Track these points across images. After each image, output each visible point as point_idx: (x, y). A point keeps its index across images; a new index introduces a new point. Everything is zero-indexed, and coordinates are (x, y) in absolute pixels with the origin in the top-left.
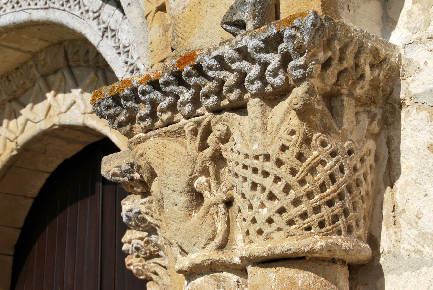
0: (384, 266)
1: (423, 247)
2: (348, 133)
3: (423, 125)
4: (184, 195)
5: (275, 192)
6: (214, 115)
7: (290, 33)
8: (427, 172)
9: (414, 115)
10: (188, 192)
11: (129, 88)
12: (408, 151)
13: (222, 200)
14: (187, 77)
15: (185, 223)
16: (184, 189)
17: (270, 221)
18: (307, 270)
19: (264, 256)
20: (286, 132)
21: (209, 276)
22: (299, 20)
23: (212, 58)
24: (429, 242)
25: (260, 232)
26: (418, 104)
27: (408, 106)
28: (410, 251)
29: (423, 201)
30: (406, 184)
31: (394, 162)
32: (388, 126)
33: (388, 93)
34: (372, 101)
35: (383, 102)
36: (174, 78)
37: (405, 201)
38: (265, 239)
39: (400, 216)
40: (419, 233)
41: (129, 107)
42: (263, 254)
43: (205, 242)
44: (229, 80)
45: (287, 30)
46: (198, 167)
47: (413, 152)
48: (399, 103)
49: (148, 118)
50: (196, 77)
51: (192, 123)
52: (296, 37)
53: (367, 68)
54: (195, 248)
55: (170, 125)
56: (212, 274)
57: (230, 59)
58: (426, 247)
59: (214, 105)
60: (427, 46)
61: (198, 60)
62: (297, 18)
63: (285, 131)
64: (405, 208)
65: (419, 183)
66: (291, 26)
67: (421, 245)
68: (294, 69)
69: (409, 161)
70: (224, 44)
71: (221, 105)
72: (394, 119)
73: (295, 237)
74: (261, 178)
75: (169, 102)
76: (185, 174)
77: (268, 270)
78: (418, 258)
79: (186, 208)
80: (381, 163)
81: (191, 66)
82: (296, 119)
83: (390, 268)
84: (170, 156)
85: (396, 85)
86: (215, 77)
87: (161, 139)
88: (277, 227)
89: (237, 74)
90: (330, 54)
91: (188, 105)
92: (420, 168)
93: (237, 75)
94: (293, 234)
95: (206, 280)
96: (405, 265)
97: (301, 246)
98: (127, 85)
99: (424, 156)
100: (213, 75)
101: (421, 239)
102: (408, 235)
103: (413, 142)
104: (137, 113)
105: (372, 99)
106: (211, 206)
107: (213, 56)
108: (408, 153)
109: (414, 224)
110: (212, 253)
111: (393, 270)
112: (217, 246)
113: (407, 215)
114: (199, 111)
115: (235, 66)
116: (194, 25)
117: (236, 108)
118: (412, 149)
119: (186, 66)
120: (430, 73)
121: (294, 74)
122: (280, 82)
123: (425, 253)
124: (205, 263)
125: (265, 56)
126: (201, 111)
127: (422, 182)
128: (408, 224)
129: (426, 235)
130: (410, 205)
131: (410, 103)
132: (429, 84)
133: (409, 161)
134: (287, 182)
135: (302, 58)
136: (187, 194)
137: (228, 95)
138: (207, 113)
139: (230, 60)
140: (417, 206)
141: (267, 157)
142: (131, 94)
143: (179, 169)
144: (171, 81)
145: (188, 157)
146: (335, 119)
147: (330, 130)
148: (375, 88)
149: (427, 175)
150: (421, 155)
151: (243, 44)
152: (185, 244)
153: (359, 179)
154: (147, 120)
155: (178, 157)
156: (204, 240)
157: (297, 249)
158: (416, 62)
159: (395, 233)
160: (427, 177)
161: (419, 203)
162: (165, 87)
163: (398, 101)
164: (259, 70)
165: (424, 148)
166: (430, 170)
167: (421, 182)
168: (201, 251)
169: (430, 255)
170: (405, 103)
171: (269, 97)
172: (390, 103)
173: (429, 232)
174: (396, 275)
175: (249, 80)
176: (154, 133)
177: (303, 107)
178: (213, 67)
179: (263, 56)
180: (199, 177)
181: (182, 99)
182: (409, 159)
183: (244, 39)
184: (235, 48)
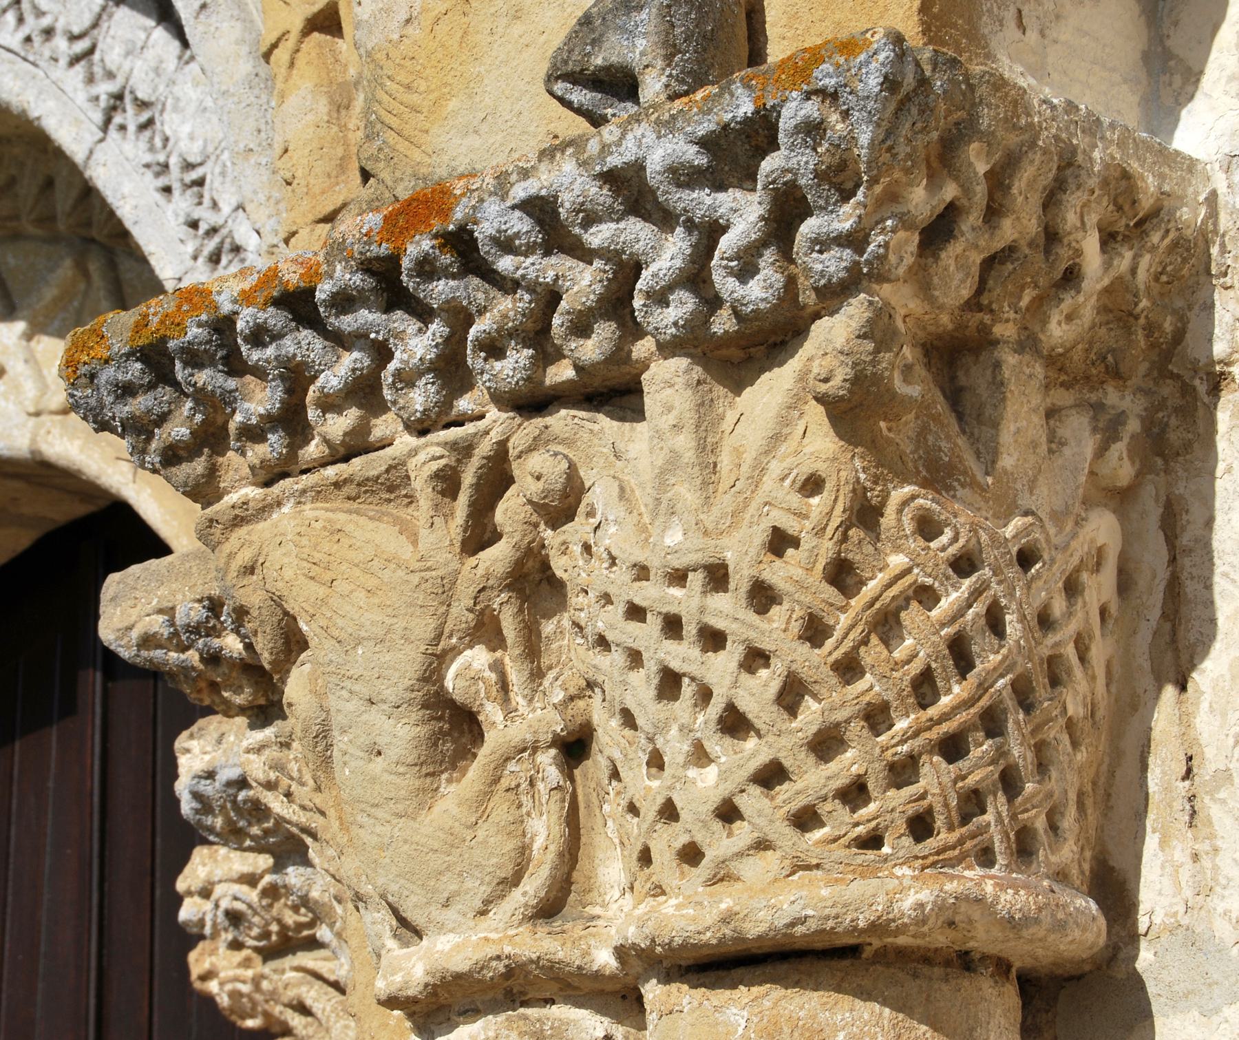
2: (1019, 486)
5: (747, 705)
6: (518, 420)
7: (802, 113)
10: (425, 706)
11: (204, 317)
13: (550, 736)
14: (418, 276)
16: (409, 695)
17: (728, 813)
18: (865, 994)
20: (788, 482)
21: (502, 1017)
22: (838, 66)
23: (513, 207)
31: (1190, 596)
32: (1166, 462)
33: (1169, 337)
34: (1107, 367)
35: (1150, 370)
36: (370, 282)
38: (710, 880)
39: (1211, 793)
41: (203, 389)
42: (702, 937)
43: (484, 891)
44: (576, 289)
45: (794, 104)
46: (461, 613)
48: (1208, 374)
49: (273, 430)
51: (438, 451)
52: (825, 130)
53: (1091, 245)
55: (356, 456)
56: (514, 1010)
57: (579, 211)
59: (521, 383)
61: (459, 214)
63: (783, 479)
64: (1231, 766)
66: (805, 87)
68: (817, 248)
70: (558, 155)
71: (548, 382)
72: (1190, 436)
73: (820, 873)
74: (695, 652)
75: (354, 370)
76: (413, 638)
79: (416, 765)
80: (1140, 597)
81: (436, 236)
82: (826, 435)
83: (1176, 988)
85: (1196, 307)
86: (523, 276)
87: (322, 509)
88: (756, 835)
89: (607, 268)
90: (950, 191)
91: (424, 380)
93: (605, 272)
94: (814, 862)
97: (845, 906)
98: (195, 308)
100: (518, 268)
104: (234, 411)
105: (1110, 358)
106: (508, 759)
107: (516, 201)
111: (1186, 996)
112: (533, 907)
114: (464, 404)
116: (446, 84)
117: (602, 394)
119: (417, 237)
121: (819, 267)
122: (764, 295)
124: (485, 972)
126: (472, 406)
135: (847, 208)
136: (420, 713)
137: (573, 345)
138: (493, 413)
139: (581, 215)
141: (717, 577)
143: (389, 621)
144: (361, 291)
145: (423, 574)
146: (972, 434)
147: (950, 475)
148: (1120, 319)
151: (629, 157)
152: (414, 899)
153: (1061, 656)
154: (269, 436)
155: (386, 575)
157: (827, 918)
159: (1196, 857)
162: (337, 316)
163: (1207, 365)
164: (688, 251)
168: (472, 924)
170: (1230, 373)
171: (724, 352)
172: (1173, 376)
174: (1196, 1013)
175: (652, 287)
178: (517, 242)
179: (702, 201)
181: (402, 361)
183: (630, 136)
184: (598, 168)
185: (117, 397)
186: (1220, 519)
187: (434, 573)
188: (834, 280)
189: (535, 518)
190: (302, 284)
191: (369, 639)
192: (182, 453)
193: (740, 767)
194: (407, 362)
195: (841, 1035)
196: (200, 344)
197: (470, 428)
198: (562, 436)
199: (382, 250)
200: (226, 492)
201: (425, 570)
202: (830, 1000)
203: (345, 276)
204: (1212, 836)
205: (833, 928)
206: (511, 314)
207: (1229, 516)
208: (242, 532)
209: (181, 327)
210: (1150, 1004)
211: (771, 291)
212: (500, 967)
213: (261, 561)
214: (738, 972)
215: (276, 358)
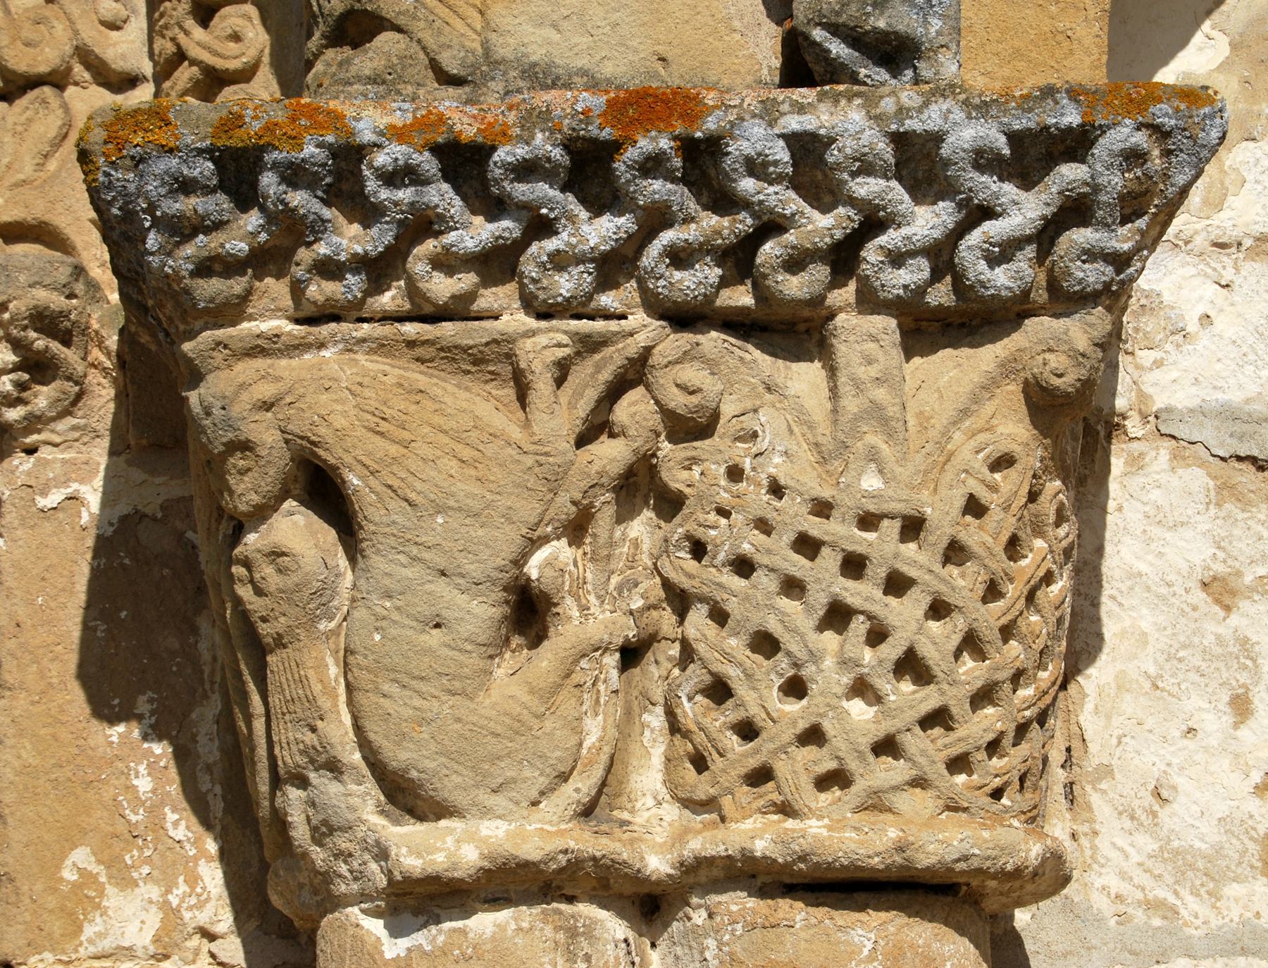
0: (1031, 941)
1: (1176, 893)
3: (1190, 512)
4: (487, 596)
5: (927, 651)
6: (668, 330)
7: (1133, 140)
8: (1197, 661)
9: (1158, 473)
10: (505, 589)
11: (330, 139)
12: (1129, 583)
13: (621, 640)
14: (638, 170)
15: (468, 703)
16: (495, 574)
17: (887, 747)
18: (961, 931)
19: (873, 869)
20: (981, 456)
21: (536, 910)
22: (1177, 110)
23: (779, 136)
24: (1198, 882)
25: (761, 776)
26: (1174, 442)
27: (1131, 439)
28: (1129, 901)
29: (1179, 750)
30: (1119, 687)
36: (566, 160)
37: (1114, 741)
40: (1161, 847)
41: (295, 209)
42: (870, 861)
43: (543, 782)
44: (810, 227)
45: (1126, 130)
46: (563, 506)
47: (1148, 589)
48: (1106, 422)
49: (356, 272)
50: (672, 182)
51: (565, 339)
52: (1146, 161)
54: (499, 801)
56: (548, 904)
58: (1185, 893)
59: (700, 298)
60: (1215, 270)
61: (711, 124)
62: (1168, 99)
63: (977, 452)
64: (1113, 763)
65: (1169, 692)
66: (1141, 119)
67: (1167, 885)
68: (1084, 258)
69: (1135, 615)
70: (843, 102)
71: (718, 303)
72: (1087, 472)
74: (878, 594)
75: (497, 238)
76: (515, 519)
77: (843, 917)
78: (1160, 928)
79: (484, 645)
81: (675, 138)
82: (1021, 421)
83: (1053, 948)
84: (446, 440)
86: (761, 202)
87: (389, 364)
88: (915, 772)
89: (856, 218)
91: (581, 268)
92: (1172, 642)
93: (853, 221)
94: (966, 805)
95: (525, 925)
96: (1111, 946)
97: (1002, 849)
99: (1188, 609)
100: (759, 193)
101: (1170, 868)
102: (1122, 850)
103: (1150, 558)
104: (317, 240)
106: (584, 656)
108: (1131, 589)
109: (1143, 817)
110: (563, 827)
112: (584, 805)
113: (1120, 786)
114: (607, 300)
115: (866, 187)
118: (1144, 578)
119: (653, 133)
120: (1220, 355)
121: (1081, 275)
122: (1012, 285)
123: (1183, 912)
124: (551, 863)
125: (994, 187)
127: (1176, 688)
128: (1120, 813)
129: (1189, 857)
130: (1132, 755)
131: (1143, 432)
132: (1215, 388)
133: (1135, 615)
134: (974, 626)
136: (500, 594)
137: (780, 278)
138: (639, 318)
139: (857, 164)
140: (1158, 762)
141: (913, 527)
142: (324, 165)
143: (489, 496)
144: (557, 165)
145: (538, 458)
149: (1198, 670)
150: (1177, 603)
151: (931, 126)
152: (456, 779)
155: (490, 450)
156: (541, 774)
157: (988, 858)
158: (1173, 308)
160: (1193, 676)
161: (1162, 752)
163: (1108, 415)
164: (951, 226)
165: (1190, 585)
166: (1207, 657)
167: (1175, 690)
168: (525, 813)
169: (1204, 923)
170: (1124, 426)
173: (1199, 849)
176: (354, 334)
177: (1077, 391)
178: (772, 169)
179: (988, 186)
180: (553, 540)
181: (568, 244)
182: (1132, 608)
183: (934, 107)
184: (894, 127)
185: (171, 192)
186: (1109, 549)
187: (551, 459)
188: (1088, 290)
189: (660, 428)
190: (480, 139)
191: (460, 509)
192: (217, 267)
193: (911, 707)
194: (574, 247)
195: (948, 964)
196: (314, 164)
197: (599, 325)
198: (709, 356)
199: (604, 134)
200: (251, 318)
201: (541, 455)
202: (940, 931)
203: (544, 145)
204: (1091, 821)
205: (989, 868)
206: (726, 232)
207: (1119, 548)
208: (260, 363)
209: (296, 141)
210: (1027, 959)
211: (1019, 282)
212: (563, 859)
213: (288, 400)
214: (861, 897)
215: (412, 204)
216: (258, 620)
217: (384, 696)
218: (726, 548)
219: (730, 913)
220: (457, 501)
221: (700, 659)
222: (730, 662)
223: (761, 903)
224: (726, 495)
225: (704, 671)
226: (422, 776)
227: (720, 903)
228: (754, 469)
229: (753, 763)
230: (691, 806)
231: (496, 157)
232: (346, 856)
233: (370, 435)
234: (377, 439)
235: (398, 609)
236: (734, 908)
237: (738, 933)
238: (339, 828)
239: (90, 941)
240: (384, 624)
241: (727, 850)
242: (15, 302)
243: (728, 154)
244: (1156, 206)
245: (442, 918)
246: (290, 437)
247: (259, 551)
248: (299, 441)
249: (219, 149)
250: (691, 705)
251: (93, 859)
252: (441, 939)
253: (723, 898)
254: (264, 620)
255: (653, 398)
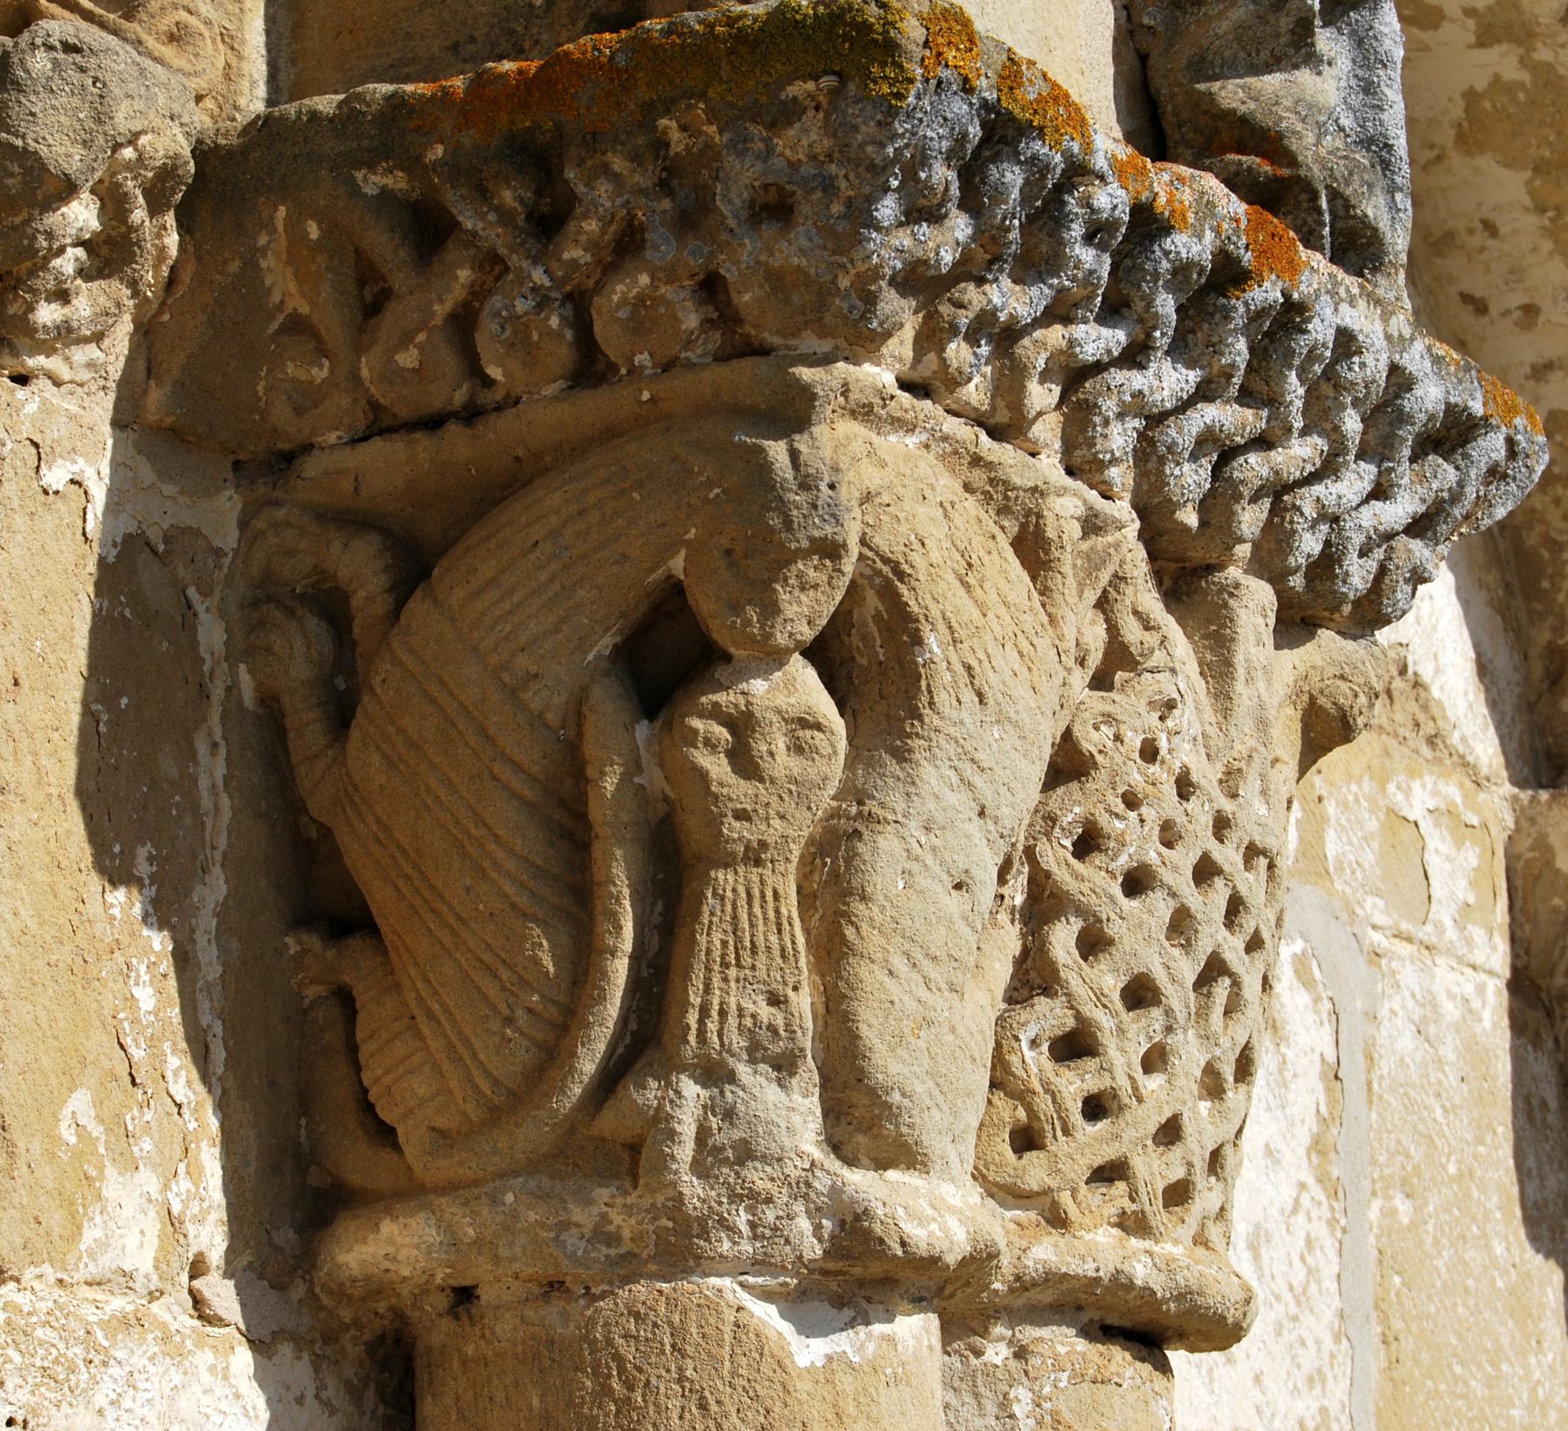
216: (730, 814)
217: (891, 973)
218: (1132, 850)
219: (1056, 1357)
220: (1017, 712)
221: (1067, 994)
222: (1105, 1006)
223: (1091, 1346)
224: (1137, 777)
225: (1070, 1012)
226: (906, 1102)
227: (1041, 1339)
228: (1170, 751)
229: (1108, 1153)
230: (1001, 1194)
231: (1167, 244)
232: (755, 1199)
233: (958, 584)
234: (962, 592)
235: (934, 849)
236: (1062, 1350)
237: (1061, 1385)
238: (764, 1156)
239: (91, 1254)
240: (914, 867)
241: (1097, 1270)
242: (149, 136)
243: (1305, 332)
244: (1461, 534)
245: (872, 1315)
246: (870, 554)
247: (779, 712)
248: (879, 564)
249: (998, 113)
250: (1033, 1054)
251: (92, 1112)
252: (871, 1348)
253: (1044, 1332)
254: (742, 815)
255: (1107, 620)
